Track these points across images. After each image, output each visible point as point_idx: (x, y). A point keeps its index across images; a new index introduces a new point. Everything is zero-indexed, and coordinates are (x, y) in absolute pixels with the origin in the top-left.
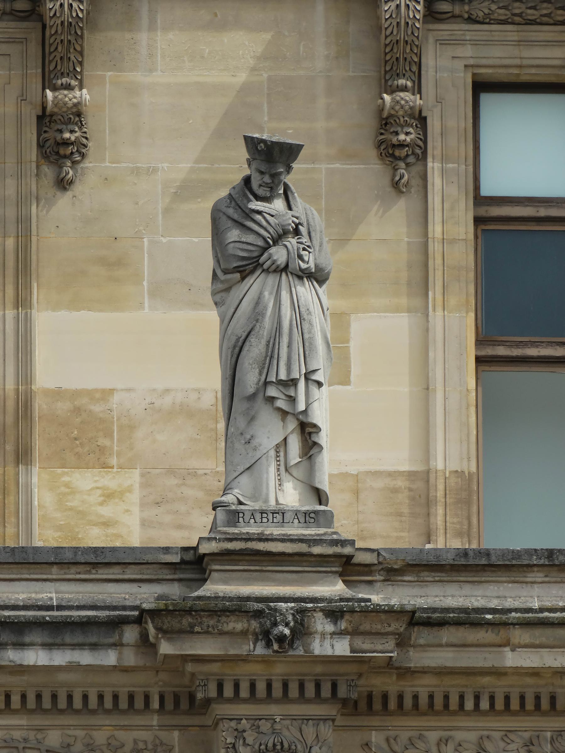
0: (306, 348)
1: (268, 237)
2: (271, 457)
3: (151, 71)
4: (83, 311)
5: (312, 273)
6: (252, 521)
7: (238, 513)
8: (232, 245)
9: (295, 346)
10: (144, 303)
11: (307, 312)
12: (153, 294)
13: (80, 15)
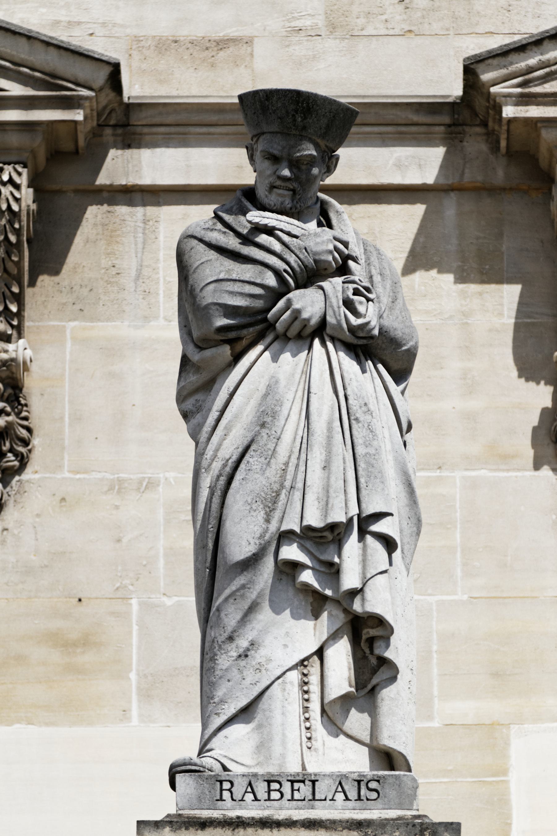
0: (361, 472)
2: (292, 683)
3: (146, 319)
4: (18, 726)
5: (372, 337)
7: (221, 782)
8: (212, 287)
9: (337, 465)
11: (365, 409)
12: (146, 695)
13: (15, 207)
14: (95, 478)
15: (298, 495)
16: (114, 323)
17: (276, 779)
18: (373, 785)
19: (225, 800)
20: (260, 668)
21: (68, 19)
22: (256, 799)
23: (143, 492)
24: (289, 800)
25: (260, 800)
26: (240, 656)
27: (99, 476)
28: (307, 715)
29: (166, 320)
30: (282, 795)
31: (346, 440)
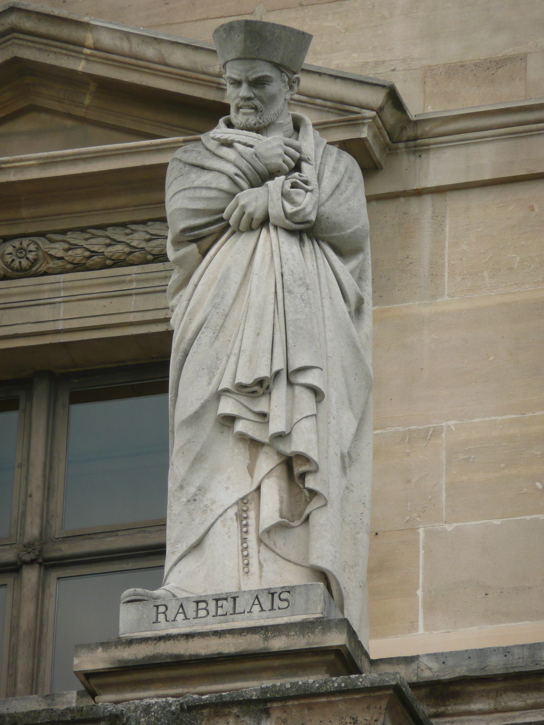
1: (236, 175)
6: (181, 617)
7: (157, 607)
10: (417, 622)
12: (430, 607)
14: (390, 432)
15: (233, 359)
16: (407, 304)
17: (204, 599)
21: (374, 59)
24: (213, 616)
25: (189, 619)
26: (189, 501)
27: (393, 429)
30: (208, 613)
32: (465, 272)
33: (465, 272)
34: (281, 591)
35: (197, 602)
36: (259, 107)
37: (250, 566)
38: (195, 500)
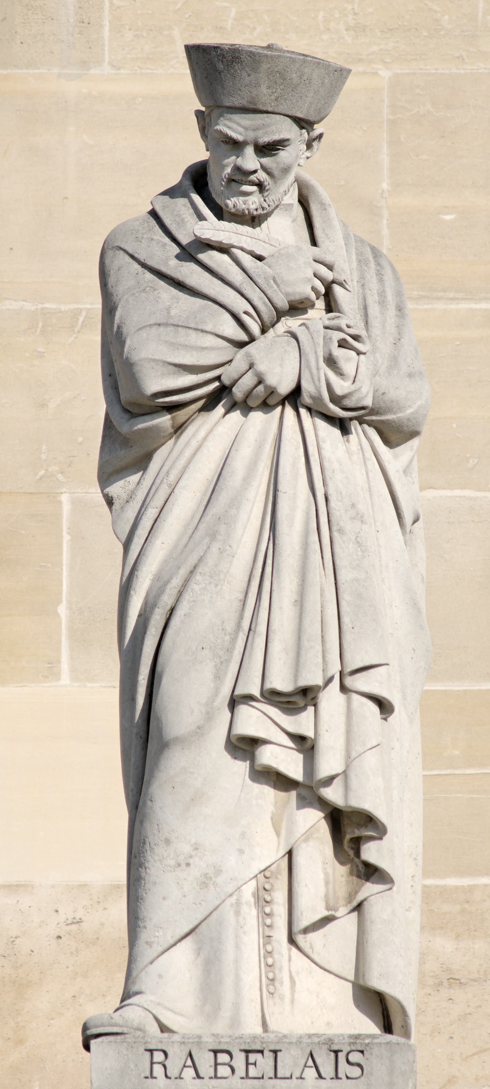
1: (245, 313)
6: (189, 1073)
9: (313, 599)
10: (59, 662)
16: (37, 71)
18: (355, 1057)
19: (156, 1078)
20: (206, 882)
22: (198, 1076)
23: (79, 332)
24: (242, 1078)
28: (269, 948)
29: (113, 66)
31: (326, 561)
32: (140, 24)
33: (140, 24)
34: (349, 1049)
35: (216, 1052)
36: (266, 183)
37: (277, 984)
38: (188, 865)
